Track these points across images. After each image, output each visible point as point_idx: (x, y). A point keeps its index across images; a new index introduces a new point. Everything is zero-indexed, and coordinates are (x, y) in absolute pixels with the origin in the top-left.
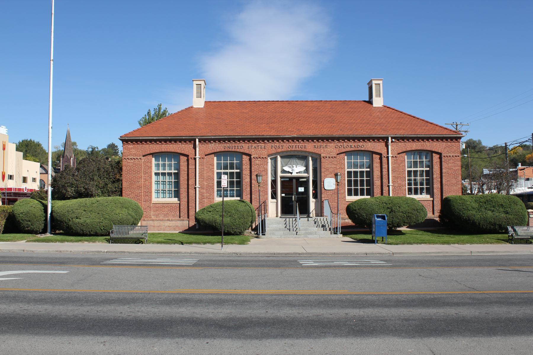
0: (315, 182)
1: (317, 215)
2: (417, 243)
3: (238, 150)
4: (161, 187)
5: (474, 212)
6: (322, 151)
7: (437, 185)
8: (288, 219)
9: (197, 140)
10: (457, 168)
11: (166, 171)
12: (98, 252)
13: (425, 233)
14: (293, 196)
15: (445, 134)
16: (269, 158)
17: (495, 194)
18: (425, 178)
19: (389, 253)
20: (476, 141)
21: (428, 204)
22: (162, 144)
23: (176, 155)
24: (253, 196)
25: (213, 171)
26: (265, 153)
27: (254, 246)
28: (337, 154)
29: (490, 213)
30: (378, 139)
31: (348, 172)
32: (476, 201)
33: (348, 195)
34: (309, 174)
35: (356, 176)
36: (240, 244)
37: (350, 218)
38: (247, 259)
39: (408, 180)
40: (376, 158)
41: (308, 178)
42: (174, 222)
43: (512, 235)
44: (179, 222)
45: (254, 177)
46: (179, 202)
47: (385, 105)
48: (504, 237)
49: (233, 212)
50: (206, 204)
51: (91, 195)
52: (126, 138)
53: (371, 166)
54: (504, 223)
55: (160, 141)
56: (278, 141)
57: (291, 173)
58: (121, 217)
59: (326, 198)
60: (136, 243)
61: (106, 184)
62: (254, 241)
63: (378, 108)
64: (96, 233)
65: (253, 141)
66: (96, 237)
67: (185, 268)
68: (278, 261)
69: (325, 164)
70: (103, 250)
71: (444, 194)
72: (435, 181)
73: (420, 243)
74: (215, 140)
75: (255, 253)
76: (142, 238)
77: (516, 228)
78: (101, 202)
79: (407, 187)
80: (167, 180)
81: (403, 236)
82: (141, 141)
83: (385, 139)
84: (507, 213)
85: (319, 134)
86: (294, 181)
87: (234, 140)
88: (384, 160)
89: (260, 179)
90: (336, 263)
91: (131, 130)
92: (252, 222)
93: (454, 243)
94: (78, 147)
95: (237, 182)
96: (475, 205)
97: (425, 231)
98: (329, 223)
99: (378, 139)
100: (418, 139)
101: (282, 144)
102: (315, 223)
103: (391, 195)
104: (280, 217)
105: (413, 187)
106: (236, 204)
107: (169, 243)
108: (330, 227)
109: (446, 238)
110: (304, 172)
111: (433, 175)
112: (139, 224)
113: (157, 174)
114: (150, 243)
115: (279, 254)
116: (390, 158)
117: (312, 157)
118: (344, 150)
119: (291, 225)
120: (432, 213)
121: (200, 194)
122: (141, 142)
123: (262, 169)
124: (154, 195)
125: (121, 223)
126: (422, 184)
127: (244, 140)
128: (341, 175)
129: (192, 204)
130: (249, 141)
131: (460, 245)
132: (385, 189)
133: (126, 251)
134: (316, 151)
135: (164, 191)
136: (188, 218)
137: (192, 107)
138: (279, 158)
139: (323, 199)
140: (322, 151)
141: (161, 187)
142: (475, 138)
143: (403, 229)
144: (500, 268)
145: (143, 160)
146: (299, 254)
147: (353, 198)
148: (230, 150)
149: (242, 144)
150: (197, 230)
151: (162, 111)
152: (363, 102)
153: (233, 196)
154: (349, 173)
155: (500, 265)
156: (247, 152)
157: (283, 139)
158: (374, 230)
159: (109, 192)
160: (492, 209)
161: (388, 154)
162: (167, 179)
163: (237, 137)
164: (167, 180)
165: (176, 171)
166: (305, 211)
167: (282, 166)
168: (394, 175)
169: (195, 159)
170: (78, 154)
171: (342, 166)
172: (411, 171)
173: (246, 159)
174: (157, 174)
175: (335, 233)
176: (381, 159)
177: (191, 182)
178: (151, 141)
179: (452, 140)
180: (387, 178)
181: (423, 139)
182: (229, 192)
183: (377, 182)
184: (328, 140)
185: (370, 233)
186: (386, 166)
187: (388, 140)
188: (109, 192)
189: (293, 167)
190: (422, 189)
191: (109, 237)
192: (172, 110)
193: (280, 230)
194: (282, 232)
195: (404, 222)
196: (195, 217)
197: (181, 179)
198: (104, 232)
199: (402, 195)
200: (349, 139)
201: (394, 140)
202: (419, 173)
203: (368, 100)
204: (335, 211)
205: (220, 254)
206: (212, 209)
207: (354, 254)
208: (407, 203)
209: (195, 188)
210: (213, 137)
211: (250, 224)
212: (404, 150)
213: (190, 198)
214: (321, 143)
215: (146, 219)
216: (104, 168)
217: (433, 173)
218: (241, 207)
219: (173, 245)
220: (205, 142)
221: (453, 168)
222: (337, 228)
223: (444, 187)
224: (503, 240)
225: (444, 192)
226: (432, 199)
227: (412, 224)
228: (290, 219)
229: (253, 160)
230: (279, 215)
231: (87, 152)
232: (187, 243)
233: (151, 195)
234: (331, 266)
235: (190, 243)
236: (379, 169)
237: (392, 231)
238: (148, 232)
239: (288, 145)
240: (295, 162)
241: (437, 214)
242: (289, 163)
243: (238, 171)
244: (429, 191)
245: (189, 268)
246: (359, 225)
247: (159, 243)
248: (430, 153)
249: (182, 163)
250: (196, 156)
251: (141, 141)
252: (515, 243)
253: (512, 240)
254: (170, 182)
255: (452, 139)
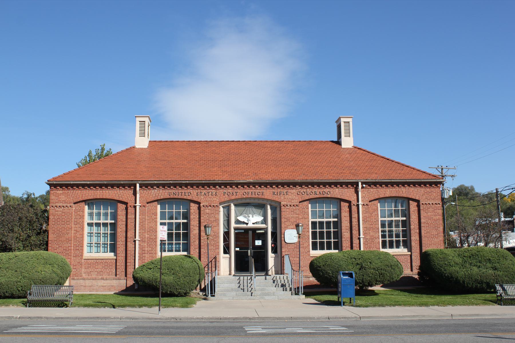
0: (274, 234)
1: (277, 273)
2: (390, 305)
3: (185, 197)
4: (94, 240)
5: (457, 269)
6: (282, 198)
7: (415, 238)
8: (242, 278)
9: (138, 185)
10: (438, 217)
11: (101, 221)
12: (9, 318)
13: (402, 293)
14: (249, 251)
15: (423, 178)
16: (221, 207)
17: (481, 247)
18: (401, 229)
19: (356, 317)
20: (468, 187)
21: (404, 259)
22: (97, 189)
23: (113, 203)
24: (202, 250)
25: (156, 222)
26: (216, 200)
27: (200, 310)
28: (300, 202)
29: (475, 269)
30: (347, 184)
31: (312, 223)
32: (459, 255)
33: (313, 249)
34: (267, 225)
35: (321, 227)
36: (183, 307)
37: (314, 275)
38: (186, 325)
39: (382, 231)
40: (345, 206)
41: (266, 230)
42: (108, 281)
43: (501, 295)
44: (115, 281)
45: (202, 228)
46: (115, 258)
47: (356, 146)
48: (493, 297)
49: (178, 269)
50: (148, 259)
51: (10, 250)
52: (55, 182)
53: (338, 215)
54: (492, 281)
55: (95, 186)
56: (231, 187)
57: (247, 224)
58: (43, 276)
59: (287, 253)
60: (59, 306)
61: (29, 236)
62: (201, 303)
63: (348, 149)
64: (12, 294)
65: (203, 187)
66: (11, 300)
67: (105, 337)
68: (220, 327)
69: (286, 213)
70: (15, 316)
71: (423, 248)
72: (412, 232)
73: (394, 305)
74: (158, 186)
75: (198, 318)
76: (67, 301)
77: (506, 287)
78: (20, 257)
79: (381, 239)
80: (102, 232)
81: (375, 297)
82: (72, 186)
83: (355, 185)
84: (495, 269)
85: (278, 178)
86: (250, 233)
87: (181, 185)
88: (354, 208)
89: (209, 230)
90: (288, 330)
91: (61, 173)
92: (199, 282)
93: (434, 305)
94: (10, 193)
95: (181, 235)
96: (459, 260)
97: (401, 290)
98: (290, 283)
99: (347, 184)
100: (392, 184)
101: (236, 190)
102: (274, 282)
103: (362, 249)
104: (234, 275)
105: (387, 239)
106: (181, 260)
107: (98, 306)
108: (291, 286)
109: (425, 298)
110: (262, 223)
111: (410, 225)
112: (67, 283)
113: (90, 225)
114: (75, 306)
115: (226, 318)
116: (360, 206)
117: (271, 206)
118: (307, 197)
119: (245, 284)
120: (410, 269)
121: (140, 248)
122: (72, 187)
123: (212, 219)
124: (86, 249)
125: (43, 282)
126: (397, 236)
127: (192, 185)
128: (302, 226)
129: (130, 260)
130: (198, 187)
131: (440, 307)
132: (355, 241)
133: (43, 316)
134: (276, 198)
135: (98, 245)
136: (126, 276)
137: (134, 147)
138: (233, 207)
139: (283, 254)
140: (282, 198)
141: (94, 240)
142: (467, 184)
143: (377, 288)
144: (480, 335)
145: (74, 209)
146: (250, 319)
147: (319, 253)
148: (176, 197)
149: (190, 190)
150: (137, 290)
151: (105, 152)
152: (331, 143)
153: (179, 251)
154: (314, 224)
155: (480, 332)
156: (196, 200)
157: (237, 185)
158: (340, 290)
159: (31, 245)
160: (478, 264)
161: (358, 201)
162: (102, 230)
163: (183, 182)
164: (102, 232)
165: (113, 221)
166: (262, 267)
167: (236, 216)
168: (365, 226)
169: (135, 207)
170: (10, 201)
171: (306, 216)
172: (330, 222)
173: (194, 207)
174: (90, 225)
175: (296, 294)
176: (350, 207)
177: (130, 234)
178: (84, 186)
179: (431, 185)
180: (357, 229)
181: (398, 184)
182: (174, 246)
183: (346, 234)
184: (289, 186)
185: (335, 293)
186: (356, 216)
187: (358, 185)
188: (31, 245)
189: (249, 217)
190: (398, 242)
191: (25, 300)
192: (116, 149)
193: (232, 290)
194: (234, 293)
195: (376, 281)
196: (133, 275)
197: (119, 230)
198: (22, 293)
199: (375, 249)
200: (313, 184)
201: (364, 185)
202: (394, 224)
203: (336, 140)
204: (296, 268)
205: (156, 319)
206: (153, 266)
207: (314, 318)
208: (379, 258)
209: (135, 241)
210: (156, 182)
211: (197, 283)
212: (377, 197)
213: (128, 252)
214: (281, 190)
215: (75, 278)
216: (26, 218)
217: (410, 223)
218: (187, 263)
219: (102, 309)
220: (147, 187)
221: (432, 217)
222: (298, 288)
223: (424, 240)
224: (491, 301)
225: (423, 245)
226: (410, 253)
227: (386, 282)
228: (244, 278)
229: (202, 209)
230: (233, 272)
231: (21, 199)
232: (119, 306)
233: (82, 250)
234: (280, 334)
235: (123, 306)
236: (348, 219)
237: (363, 291)
238: (74, 293)
239: (243, 191)
240: (251, 211)
241: (416, 271)
242: (244, 212)
243: (185, 221)
244: (407, 244)
245: (109, 337)
246: (324, 284)
247: (86, 306)
248: (406, 201)
249: (119, 212)
250: (136, 203)
251: (72, 186)
252: (504, 305)
253: (501, 300)
254: (105, 234)
255: (431, 184)
